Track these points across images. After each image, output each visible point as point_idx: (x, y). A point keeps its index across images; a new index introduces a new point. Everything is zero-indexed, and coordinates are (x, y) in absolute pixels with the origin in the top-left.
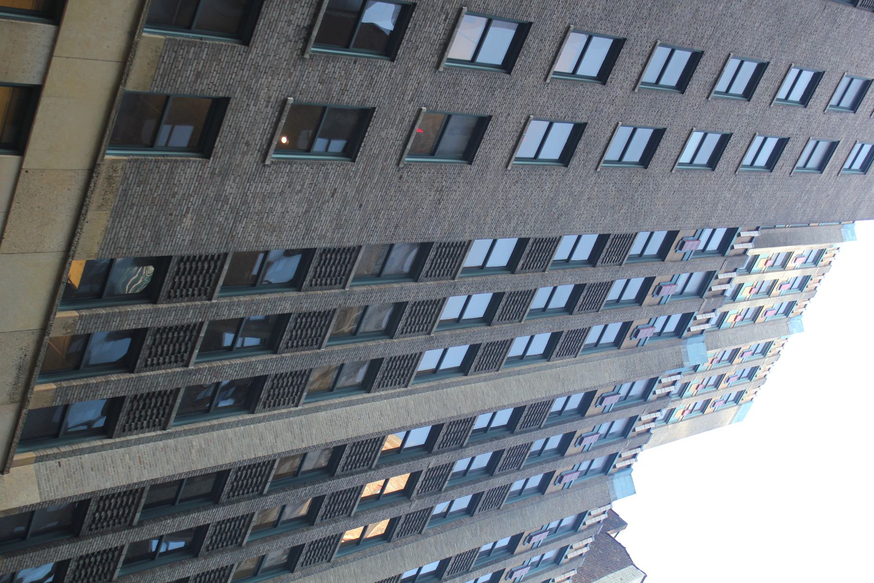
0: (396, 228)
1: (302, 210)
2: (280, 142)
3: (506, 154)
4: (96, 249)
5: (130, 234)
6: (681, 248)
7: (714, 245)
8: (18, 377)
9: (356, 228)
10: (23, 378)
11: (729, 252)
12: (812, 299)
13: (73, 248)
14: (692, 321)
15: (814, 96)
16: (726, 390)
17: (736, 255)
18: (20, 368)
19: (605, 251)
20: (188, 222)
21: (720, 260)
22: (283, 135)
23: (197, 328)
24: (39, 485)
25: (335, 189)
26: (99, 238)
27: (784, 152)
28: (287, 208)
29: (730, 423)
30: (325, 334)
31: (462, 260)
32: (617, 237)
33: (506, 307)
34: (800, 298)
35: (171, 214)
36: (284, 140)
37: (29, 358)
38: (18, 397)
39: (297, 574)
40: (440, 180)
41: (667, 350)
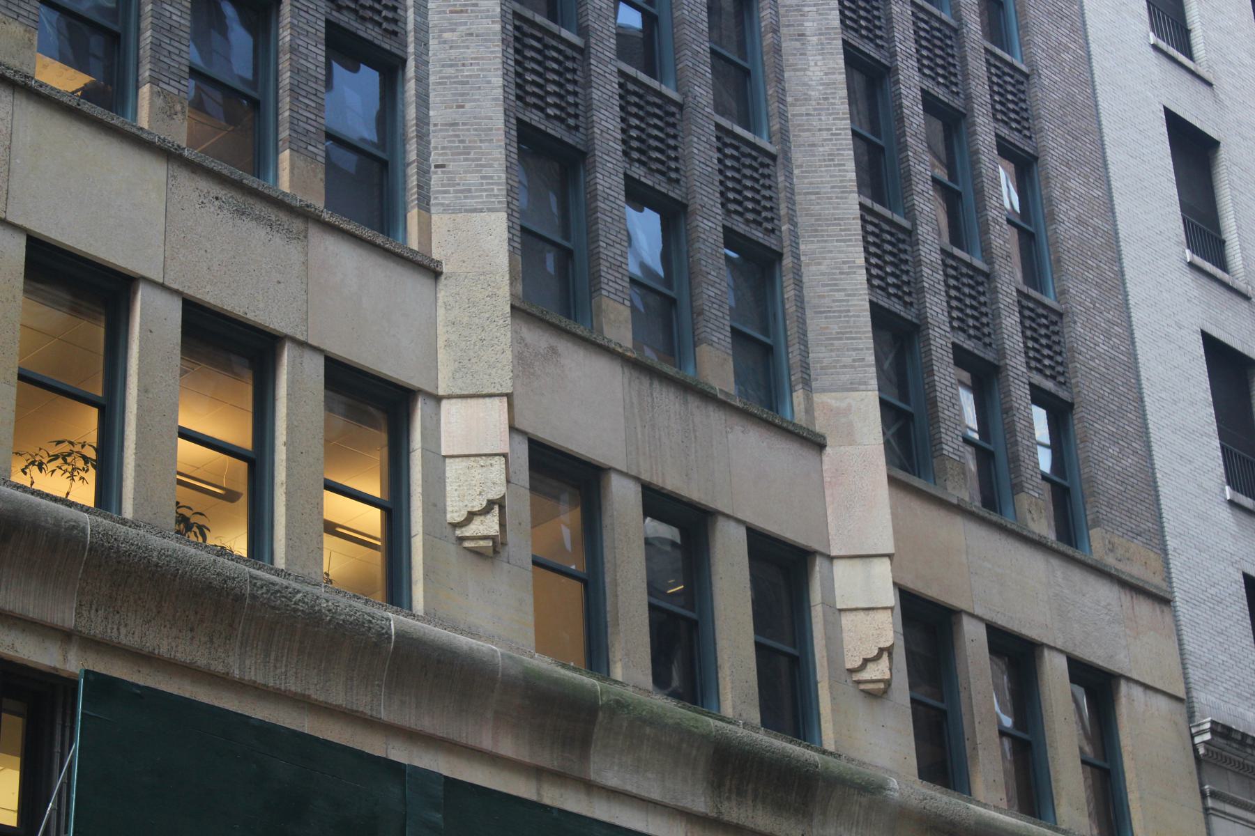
8: (258, 219)
10: (260, 208)
18: (241, 213)
24: (475, 211)
37: (216, 190)
38: (298, 224)
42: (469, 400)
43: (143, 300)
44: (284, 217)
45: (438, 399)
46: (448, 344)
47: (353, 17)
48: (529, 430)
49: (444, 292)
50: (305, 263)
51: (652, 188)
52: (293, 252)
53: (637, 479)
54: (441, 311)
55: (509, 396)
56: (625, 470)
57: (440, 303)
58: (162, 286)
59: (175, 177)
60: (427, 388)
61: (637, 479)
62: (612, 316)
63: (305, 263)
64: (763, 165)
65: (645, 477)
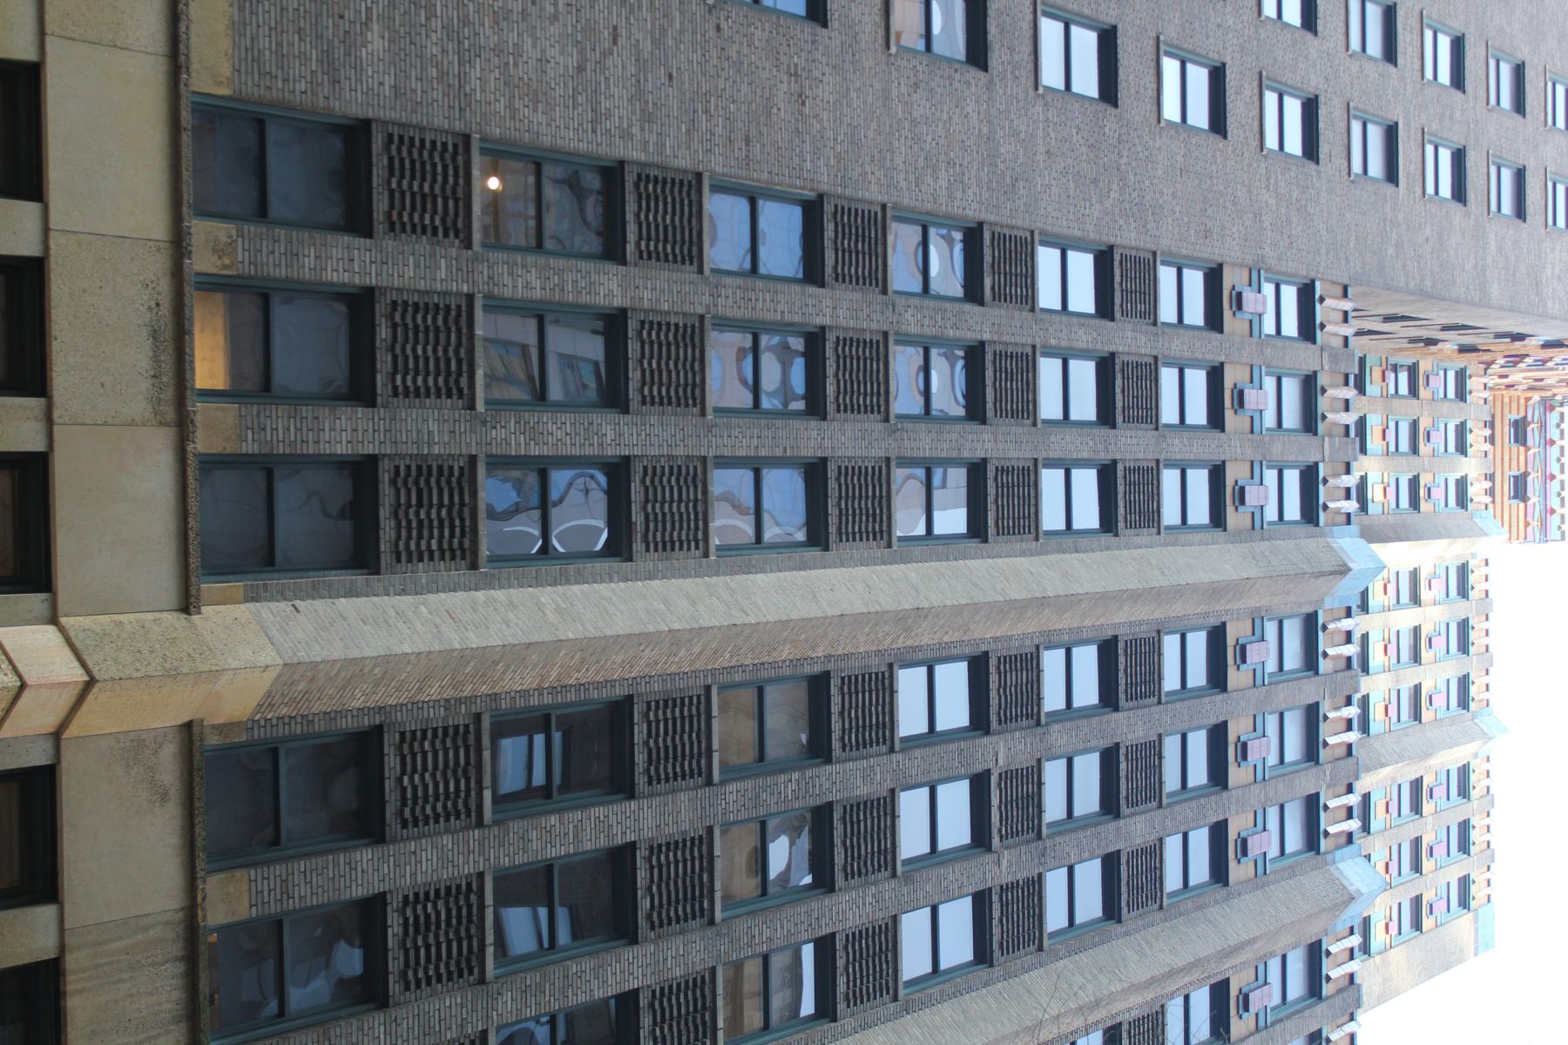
0: (747, 144)
1: (573, 62)
2: (486, 190)
3: (878, 19)
4: (225, 69)
5: (279, 45)
6: (1246, 1009)
7: (1296, 988)
8: (156, 359)
9: (679, 128)
10: (168, 359)
11: (1327, 989)
12: (1493, 866)
13: (182, 46)
14: (1322, 813)
15: (1320, 14)
16: (1439, 878)
17: (1339, 991)
18: (155, 335)
19: (1124, 889)
20: (376, 40)
21: (1321, 1008)
22: (487, 174)
23: (471, 728)
24: (270, 639)
25: (615, 28)
26: (224, 44)
27: (1321, 125)
28: (544, 51)
29: (1476, 954)
30: (714, 1001)
31: (896, 971)
32: (1134, 854)
33: (1005, 808)
34: (1472, 665)
35: (341, 17)
36: (494, 183)
37: (166, 309)
38: (170, 414)
39: (846, 1022)
40: (785, 49)
41: (1312, 881)
42: (67, 651)
43: (45, 914)
44: (169, 394)
45: (53, 620)
46: (119, 624)
47: (386, 208)
48: (64, 763)
49: (173, 619)
50: (133, 423)
51: (386, 950)
52: (139, 407)
53: (62, 948)
54: (150, 616)
55: (91, 683)
56: (67, 926)
57: (158, 615)
58: (46, 230)
59: (159, 250)
60: (61, 599)
61: (62, 948)
62: (231, 889)
63: (133, 423)
64: (463, 551)
65: (70, 962)
